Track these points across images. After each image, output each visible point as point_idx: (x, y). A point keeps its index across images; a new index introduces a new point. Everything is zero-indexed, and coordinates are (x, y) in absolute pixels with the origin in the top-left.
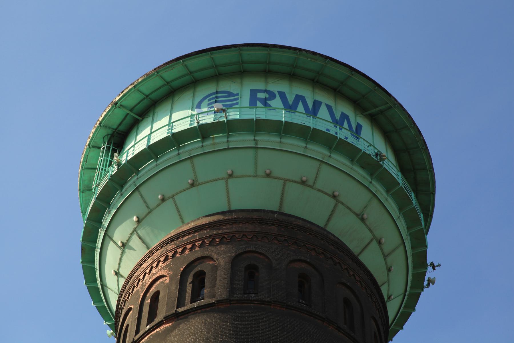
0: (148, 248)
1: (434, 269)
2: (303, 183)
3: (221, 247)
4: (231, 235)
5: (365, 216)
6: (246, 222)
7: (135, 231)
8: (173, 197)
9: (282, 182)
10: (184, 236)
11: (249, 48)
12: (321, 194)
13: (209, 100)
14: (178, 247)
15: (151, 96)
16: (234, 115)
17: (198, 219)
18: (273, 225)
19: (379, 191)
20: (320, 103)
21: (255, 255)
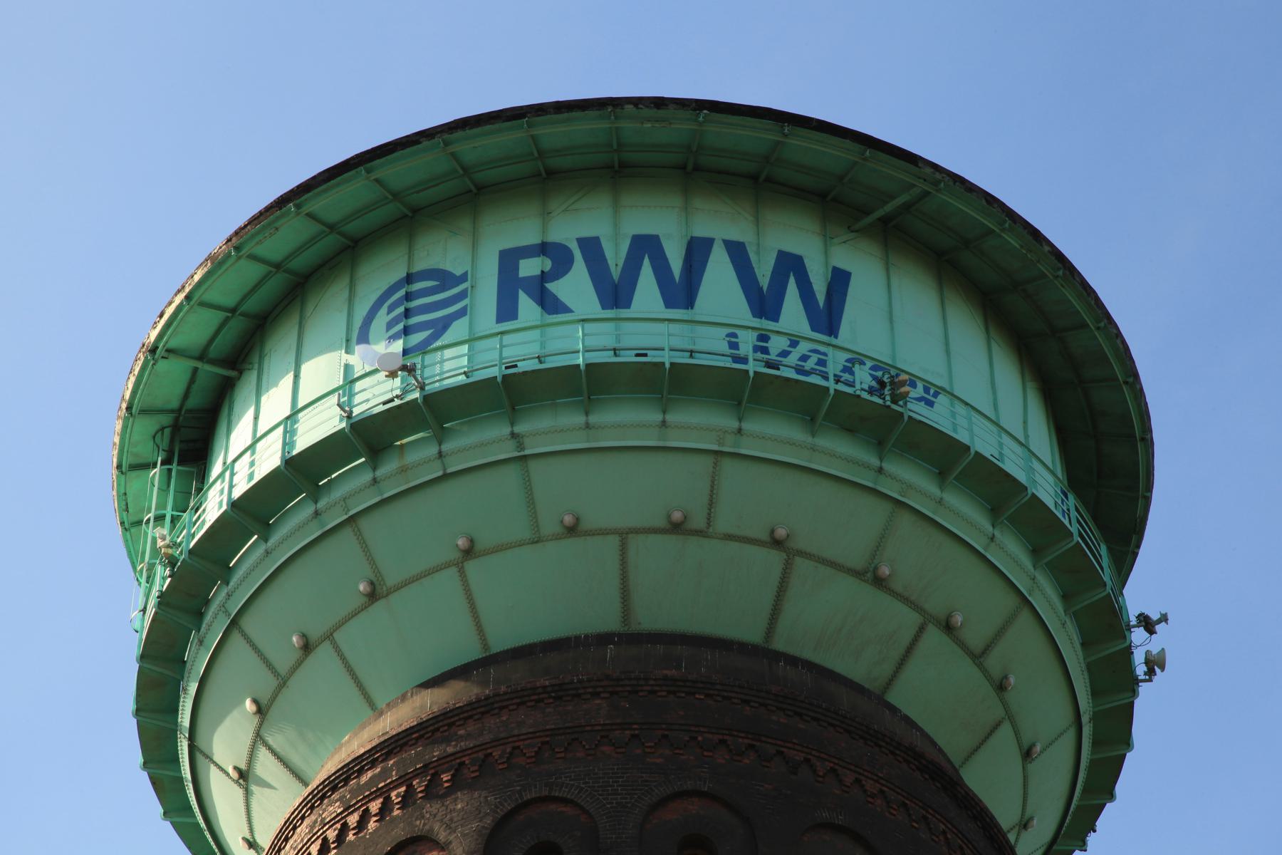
0: (306, 784)
1: (1151, 631)
2: (676, 528)
3: (456, 800)
4: (481, 755)
5: (885, 571)
6: (519, 704)
7: (258, 738)
8: (329, 636)
9: (614, 541)
10: (361, 772)
11: (469, 132)
12: (734, 546)
13: (390, 310)
14: (348, 809)
15: (243, 308)
16: (450, 366)
17: (403, 698)
18: (596, 695)
19: (910, 486)
20: (708, 243)
21: (553, 807)
